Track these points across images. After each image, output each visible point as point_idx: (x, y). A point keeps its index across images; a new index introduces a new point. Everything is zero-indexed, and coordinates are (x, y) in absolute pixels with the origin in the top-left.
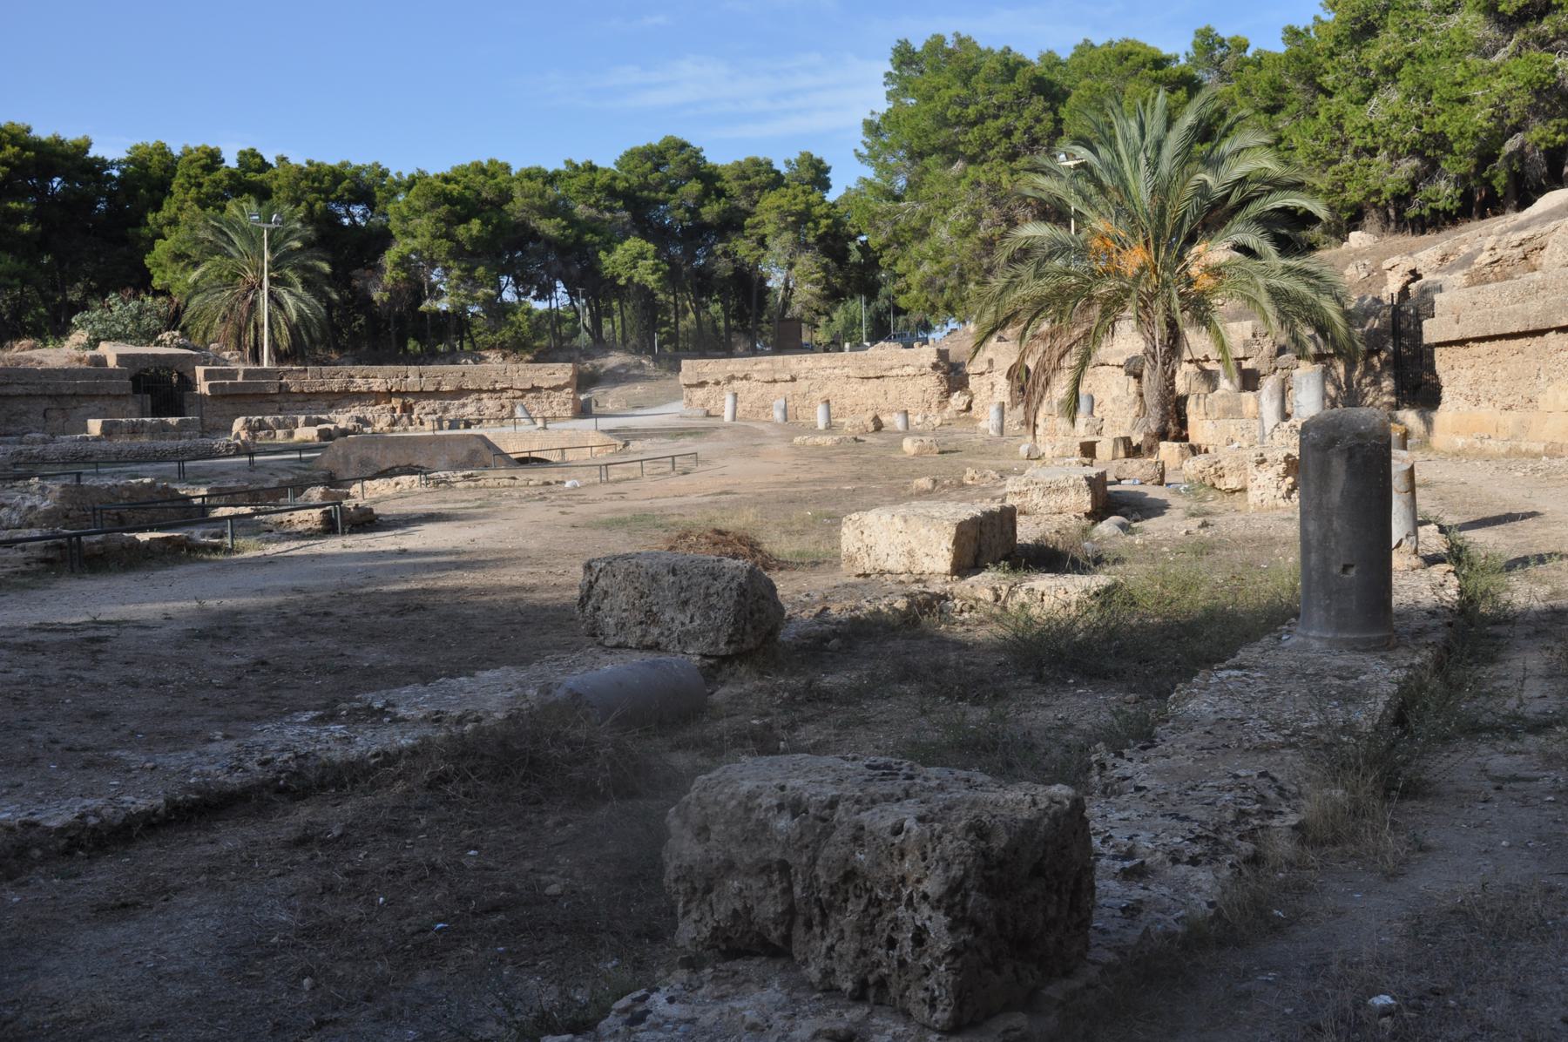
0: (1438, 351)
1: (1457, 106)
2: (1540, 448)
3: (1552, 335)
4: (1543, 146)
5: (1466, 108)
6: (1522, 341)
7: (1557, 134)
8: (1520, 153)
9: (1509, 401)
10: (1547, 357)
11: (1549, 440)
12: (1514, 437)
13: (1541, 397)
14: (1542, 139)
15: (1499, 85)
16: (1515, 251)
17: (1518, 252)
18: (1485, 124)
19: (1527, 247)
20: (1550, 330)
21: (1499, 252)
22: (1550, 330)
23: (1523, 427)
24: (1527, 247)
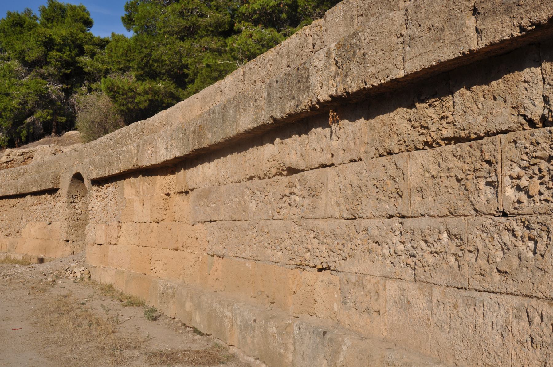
0: (329, 129)
1: (4, 97)
2: (20, 258)
3: (29, 197)
4: (41, 120)
5: (9, 98)
6: (15, 200)
7: (47, 115)
8: (33, 123)
9: (8, 231)
10: (26, 208)
11: (25, 253)
12: (9, 251)
13: (22, 230)
14: (41, 117)
15: (23, 90)
16: (19, 157)
17: (21, 158)
18: (16, 106)
19: (26, 156)
20: (27, 194)
21: (12, 157)
22: (27, 194)
23: (14, 246)
24: (26, 156)
